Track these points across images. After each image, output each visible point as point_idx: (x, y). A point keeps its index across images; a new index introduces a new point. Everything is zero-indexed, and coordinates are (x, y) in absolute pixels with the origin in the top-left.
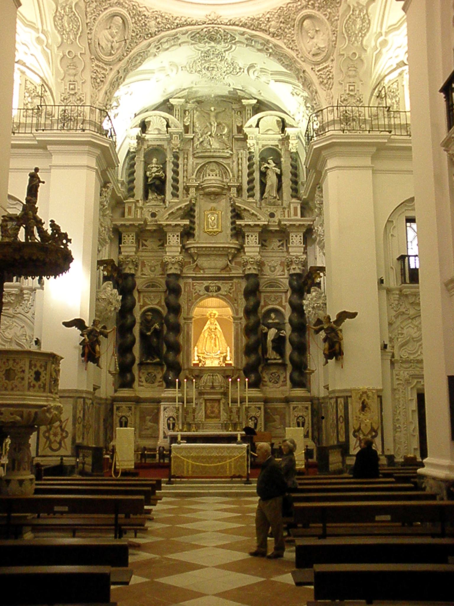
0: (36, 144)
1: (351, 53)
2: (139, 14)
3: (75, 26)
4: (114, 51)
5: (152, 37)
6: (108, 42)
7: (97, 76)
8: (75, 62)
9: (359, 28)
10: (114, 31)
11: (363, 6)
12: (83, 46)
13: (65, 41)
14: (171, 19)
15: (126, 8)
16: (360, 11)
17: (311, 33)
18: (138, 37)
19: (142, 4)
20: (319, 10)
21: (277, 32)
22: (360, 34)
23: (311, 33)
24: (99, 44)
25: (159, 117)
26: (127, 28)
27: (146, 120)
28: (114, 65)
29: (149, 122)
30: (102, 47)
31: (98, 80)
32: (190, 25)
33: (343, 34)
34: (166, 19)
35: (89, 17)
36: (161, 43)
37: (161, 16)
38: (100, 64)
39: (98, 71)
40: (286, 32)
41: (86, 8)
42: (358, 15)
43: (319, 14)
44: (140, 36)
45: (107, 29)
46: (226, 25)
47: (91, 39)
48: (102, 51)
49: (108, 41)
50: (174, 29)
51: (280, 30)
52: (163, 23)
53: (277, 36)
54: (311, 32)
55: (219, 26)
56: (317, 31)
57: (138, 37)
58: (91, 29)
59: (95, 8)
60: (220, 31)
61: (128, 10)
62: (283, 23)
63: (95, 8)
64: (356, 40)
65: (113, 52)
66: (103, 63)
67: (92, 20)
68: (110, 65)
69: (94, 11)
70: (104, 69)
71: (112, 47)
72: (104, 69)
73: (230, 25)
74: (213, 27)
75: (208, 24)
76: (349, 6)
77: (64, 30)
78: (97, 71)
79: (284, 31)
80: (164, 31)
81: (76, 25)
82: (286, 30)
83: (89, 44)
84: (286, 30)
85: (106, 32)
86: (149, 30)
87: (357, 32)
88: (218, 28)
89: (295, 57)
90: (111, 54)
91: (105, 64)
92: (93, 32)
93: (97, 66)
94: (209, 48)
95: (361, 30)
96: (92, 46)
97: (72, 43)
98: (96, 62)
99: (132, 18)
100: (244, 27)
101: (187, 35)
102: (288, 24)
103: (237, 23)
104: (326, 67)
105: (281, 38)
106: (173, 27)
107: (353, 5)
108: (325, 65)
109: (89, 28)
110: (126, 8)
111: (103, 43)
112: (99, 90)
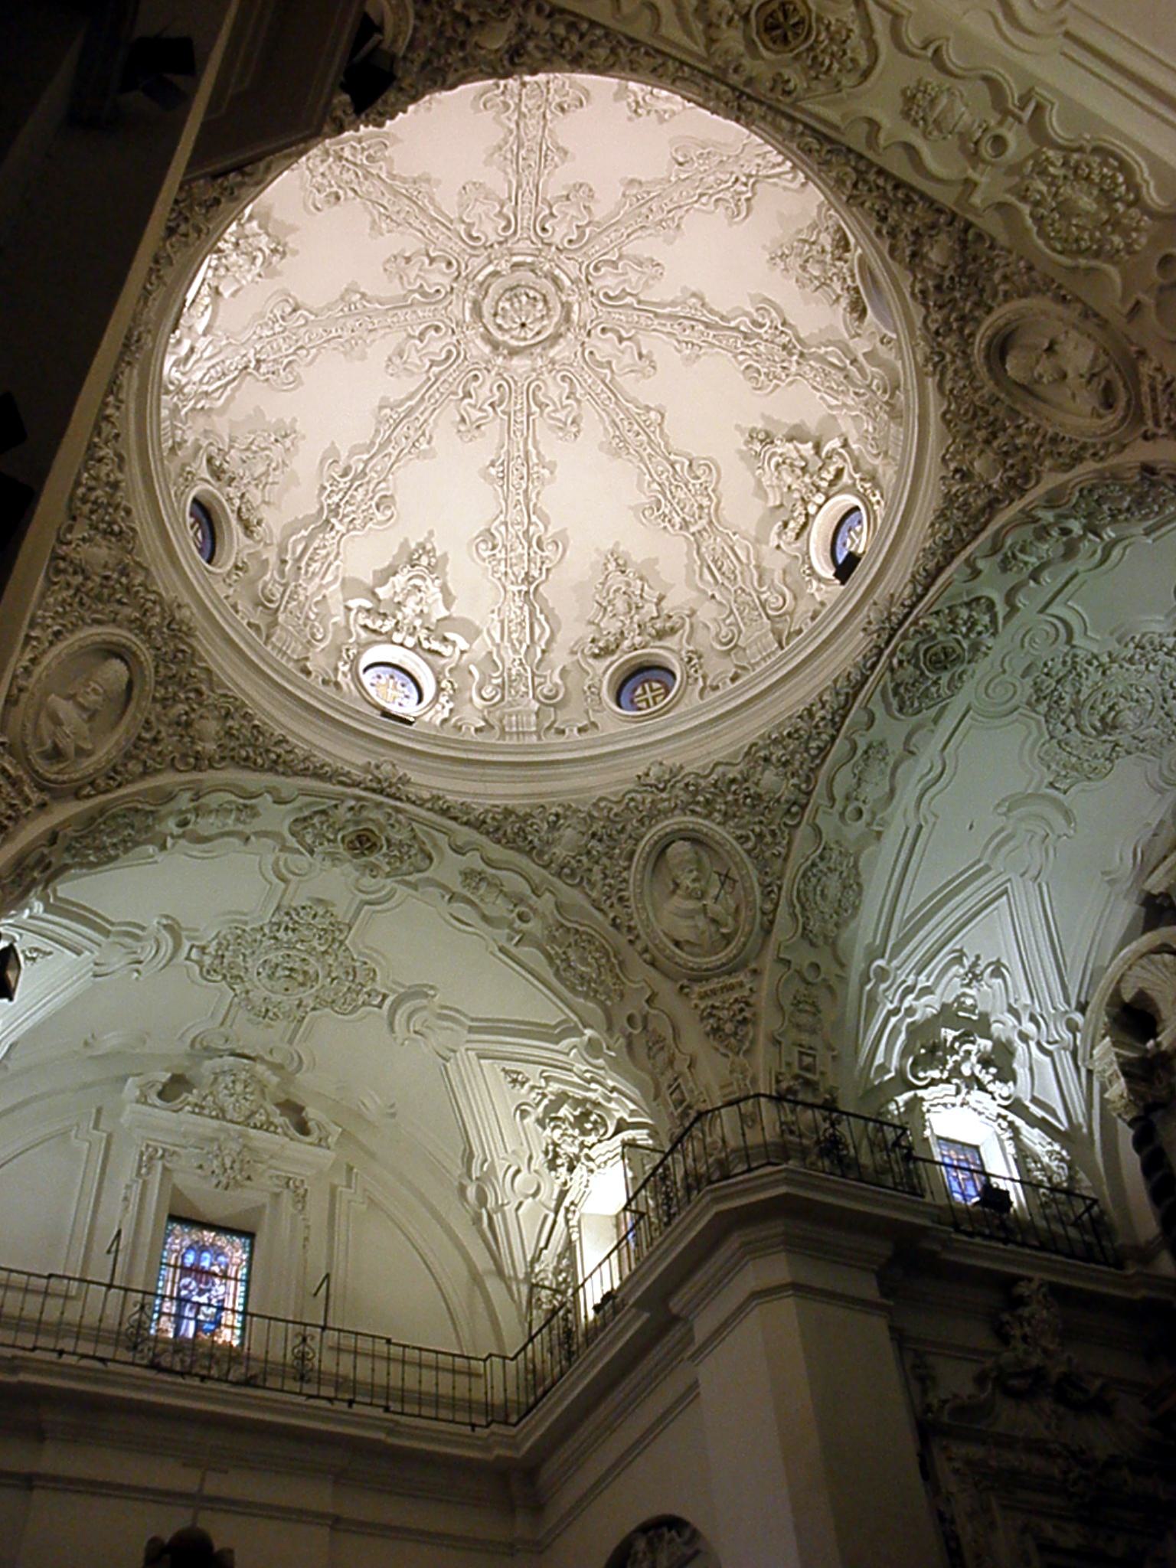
0: (648, 1320)
1: (1155, 276)
2: (722, 787)
3: (597, 955)
4: (726, 926)
5: (803, 807)
6: (692, 918)
7: (720, 1019)
8: (654, 1031)
9: (1097, 200)
10: (688, 882)
11: (1035, 156)
12: (641, 976)
13: (609, 1003)
14: (801, 724)
15: (673, 810)
16: (1043, 173)
17: (1045, 368)
18: (769, 839)
19: (704, 767)
20: (990, 310)
21: (1012, 474)
22: (1120, 206)
23: (1045, 368)
24: (677, 944)
25: (1144, 962)
26: (716, 847)
27: (1128, 996)
28: (758, 956)
29: (1141, 995)
30: (688, 942)
31: (729, 1027)
32: (317, 775)
33: (1075, 269)
34: (789, 735)
35: (605, 906)
36: (848, 798)
37: (775, 742)
38: (714, 984)
39: (717, 1004)
40: (1025, 446)
41: (588, 896)
42: (1050, 185)
43: (1002, 313)
44: (773, 833)
45: (673, 892)
46: (921, 597)
47: (646, 950)
48: (697, 950)
49: (690, 915)
50: (833, 738)
51: (1010, 462)
52: (793, 753)
53: (1026, 477)
54: (1039, 369)
55: (911, 619)
56: (1050, 349)
57: (769, 839)
58: (630, 929)
59: (606, 877)
60: (925, 626)
61: (683, 810)
62: (995, 436)
63: (606, 877)
64: (1125, 233)
65: (724, 930)
66: (718, 976)
67: (617, 906)
68: (744, 965)
69: (610, 885)
70: (731, 988)
71: (714, 921)
72: (731, 988)
73: (927, 589)
74: (904, 637)
75: (888, 643)
76: (1001, 206)
77: (589, 982)
78: (713, 1007)
79: (1017, 449)
80: (819, 766)
81: (597, 950)
82: (1019, 441)
83: (653, 963)
84: (1019, 441)
85: (679, 902)
86: (778, 801)
87: (1105, 216)
88: (915, 623)
89: (1099, 466)
90: (728, 939)
91: (729, 973)
92: (640, 930)
93: (703, 996)
94: (1029, 681)
95: (1107, 197)
96: (662, 960)
97: (622, 996)
98: (697, 988)
99: (708, 816)
100: (953, 556)
101: (289, 806)
102: (1005, 429)
103: (931, 566)
104: (1153, 389)
105: (1038, 473)
106: (825, 737)
107: (1009, 191)
108: (1145, 388)
109: (625, 930)
110: (673, 810)
111: (684, 932)
112: (747, 1052)
